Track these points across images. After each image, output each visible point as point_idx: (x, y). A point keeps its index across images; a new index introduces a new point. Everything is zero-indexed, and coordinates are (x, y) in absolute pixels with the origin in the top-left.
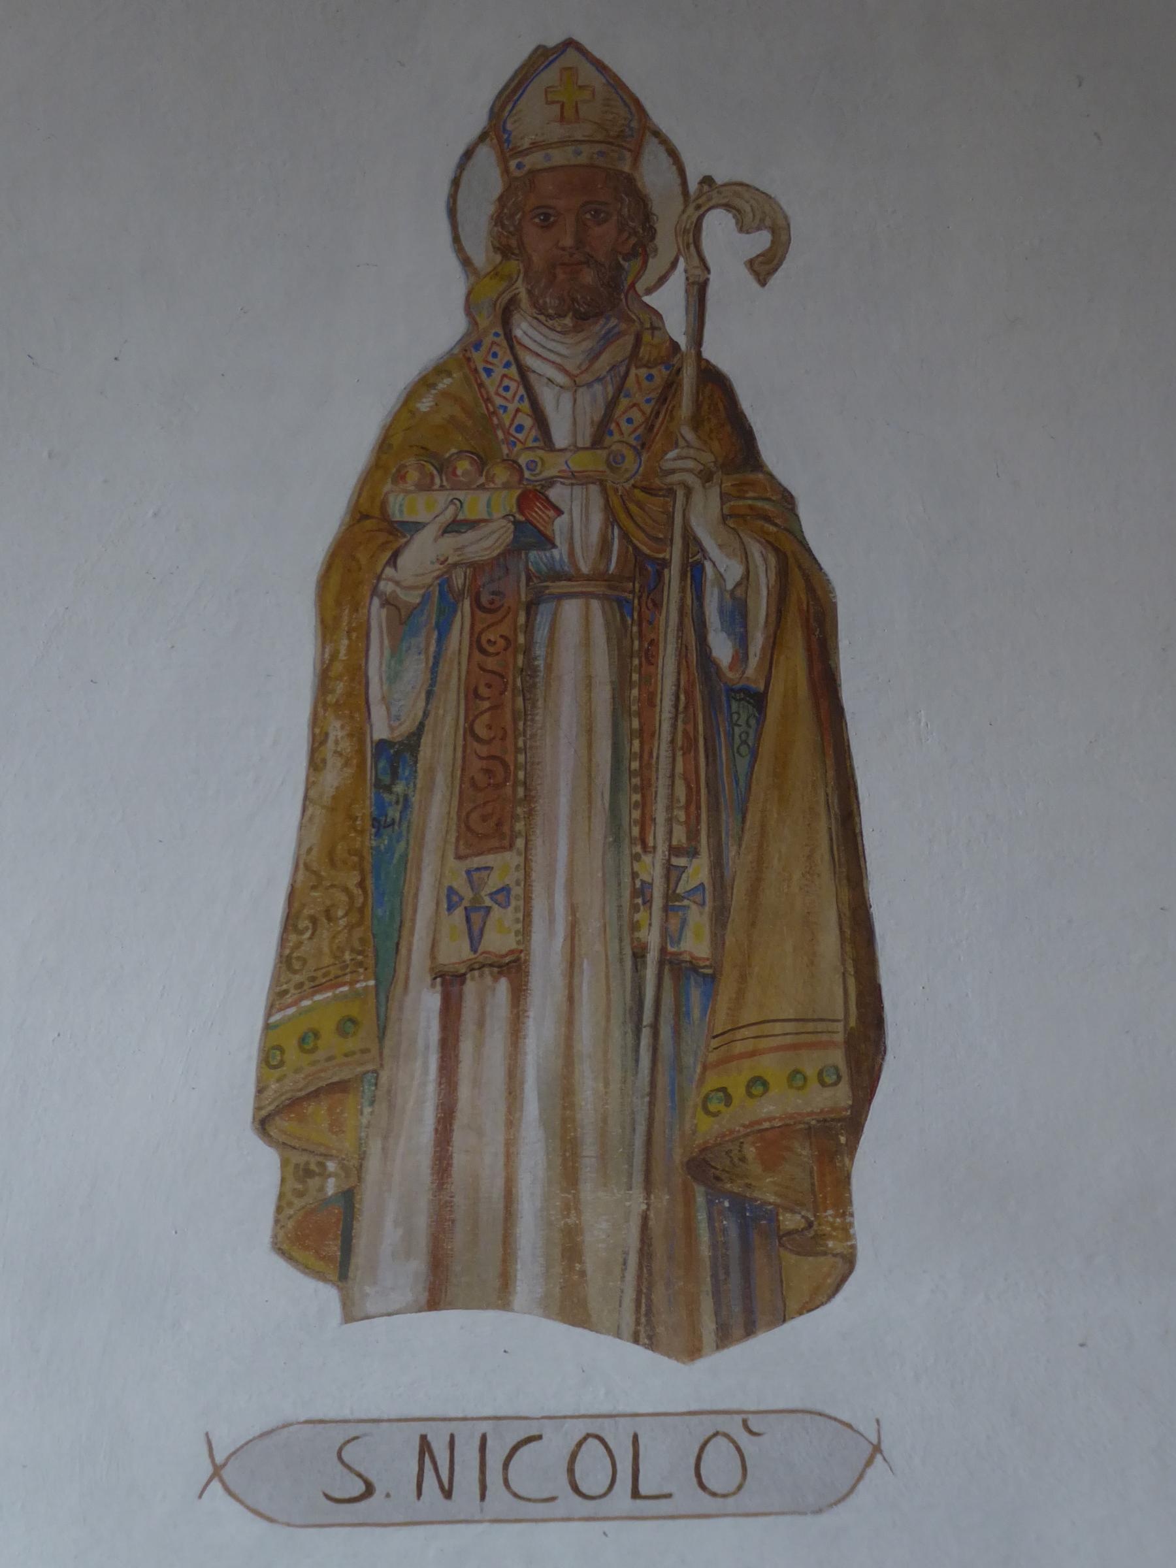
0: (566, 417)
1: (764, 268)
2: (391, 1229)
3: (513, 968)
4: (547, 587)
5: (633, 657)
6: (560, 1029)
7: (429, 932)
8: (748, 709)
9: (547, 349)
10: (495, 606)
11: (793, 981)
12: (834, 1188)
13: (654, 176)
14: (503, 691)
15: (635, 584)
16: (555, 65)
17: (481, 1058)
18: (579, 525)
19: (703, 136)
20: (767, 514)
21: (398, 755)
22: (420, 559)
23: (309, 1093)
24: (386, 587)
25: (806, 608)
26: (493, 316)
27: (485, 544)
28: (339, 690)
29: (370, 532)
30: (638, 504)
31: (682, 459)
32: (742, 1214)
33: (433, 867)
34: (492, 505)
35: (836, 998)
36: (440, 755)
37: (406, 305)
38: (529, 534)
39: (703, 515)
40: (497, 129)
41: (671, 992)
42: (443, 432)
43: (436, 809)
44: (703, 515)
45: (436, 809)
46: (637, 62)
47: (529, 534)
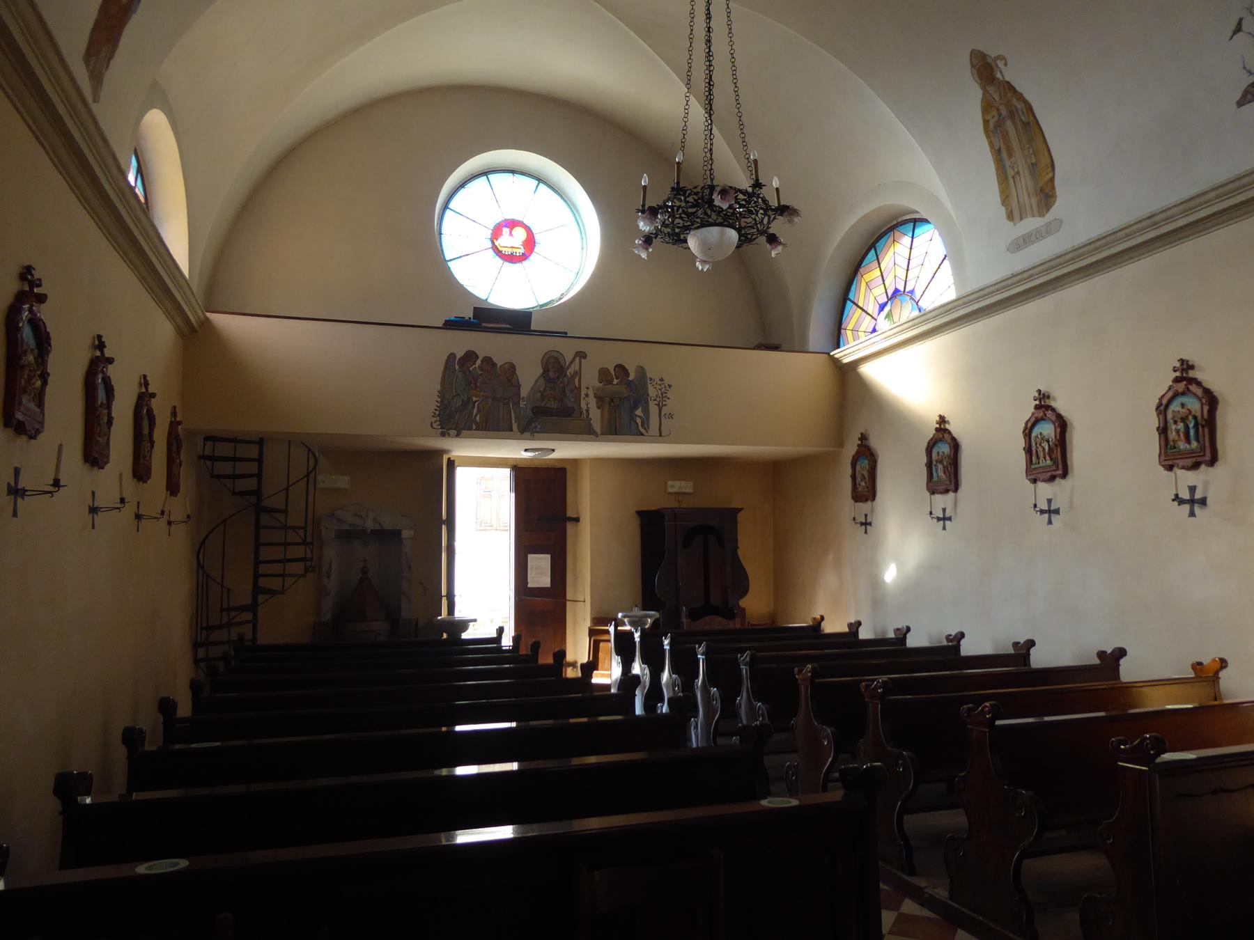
0: (996, 96)
1: (1006, 64)
2: (1016, 212)
3: (1018, 173)
4: (873, 681)
5: (1014, 123)
6: (1026, 181)
7: (1010, 173)
8: (1030, 127)
9: (990, 89)
10: (1000, 124)
11: (1044, 161)
12: (1053, 188)
13: (989, 60)
14: (1005, 136)
15: (1012, 114)
16: (972, 52)
17: (1019, 186)
18: (1003, 109)
19: (992, 53)
20: (1020, 97)
21: (999, 150)
22: (991, 125)
23: (1005, 200)
24: (839, 784)
25: (1030, 108)
26: (984, 88)
27: (996, 118)
28: (992, 146)
29: (986, 123)
30: (1008, 104)
31: (1010, 94)
32: (1046, 196)
33: (1008, 163)
34: (994, 113)
35: (1048, 161)
36: (1003, 149)
37: (975, 93)
38: (1000, 115)
39: (1014, 101)
40: (972, 66)
41: (1033, 168)
42: (987, 107)
43: (1004, 154)
44: (1014, 101)
45: (1004, 154)
46: (980, 48)
47: (1000, 115)
